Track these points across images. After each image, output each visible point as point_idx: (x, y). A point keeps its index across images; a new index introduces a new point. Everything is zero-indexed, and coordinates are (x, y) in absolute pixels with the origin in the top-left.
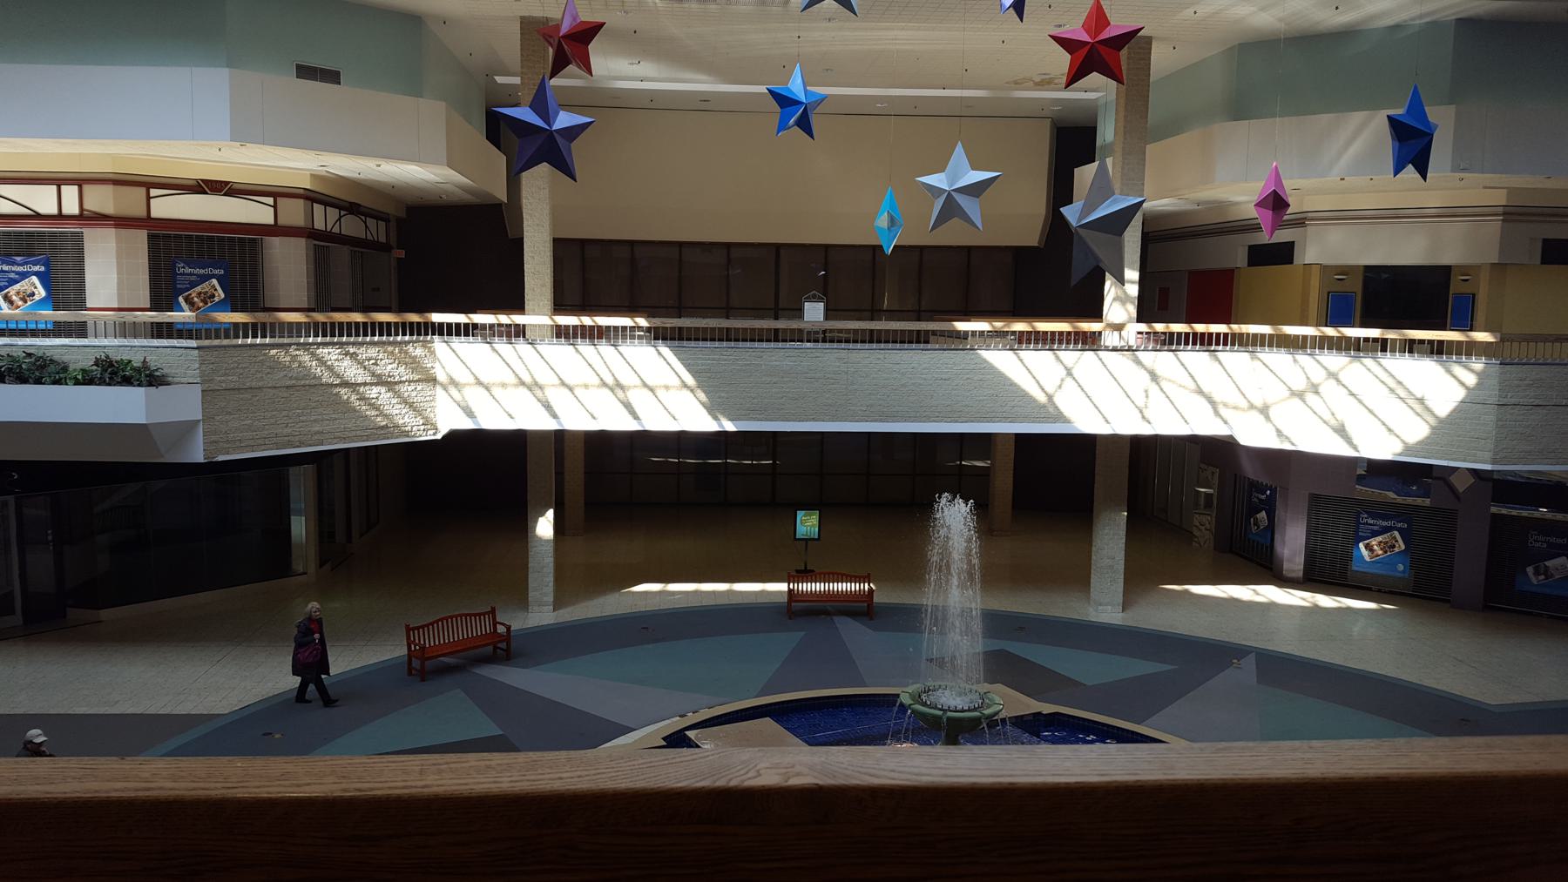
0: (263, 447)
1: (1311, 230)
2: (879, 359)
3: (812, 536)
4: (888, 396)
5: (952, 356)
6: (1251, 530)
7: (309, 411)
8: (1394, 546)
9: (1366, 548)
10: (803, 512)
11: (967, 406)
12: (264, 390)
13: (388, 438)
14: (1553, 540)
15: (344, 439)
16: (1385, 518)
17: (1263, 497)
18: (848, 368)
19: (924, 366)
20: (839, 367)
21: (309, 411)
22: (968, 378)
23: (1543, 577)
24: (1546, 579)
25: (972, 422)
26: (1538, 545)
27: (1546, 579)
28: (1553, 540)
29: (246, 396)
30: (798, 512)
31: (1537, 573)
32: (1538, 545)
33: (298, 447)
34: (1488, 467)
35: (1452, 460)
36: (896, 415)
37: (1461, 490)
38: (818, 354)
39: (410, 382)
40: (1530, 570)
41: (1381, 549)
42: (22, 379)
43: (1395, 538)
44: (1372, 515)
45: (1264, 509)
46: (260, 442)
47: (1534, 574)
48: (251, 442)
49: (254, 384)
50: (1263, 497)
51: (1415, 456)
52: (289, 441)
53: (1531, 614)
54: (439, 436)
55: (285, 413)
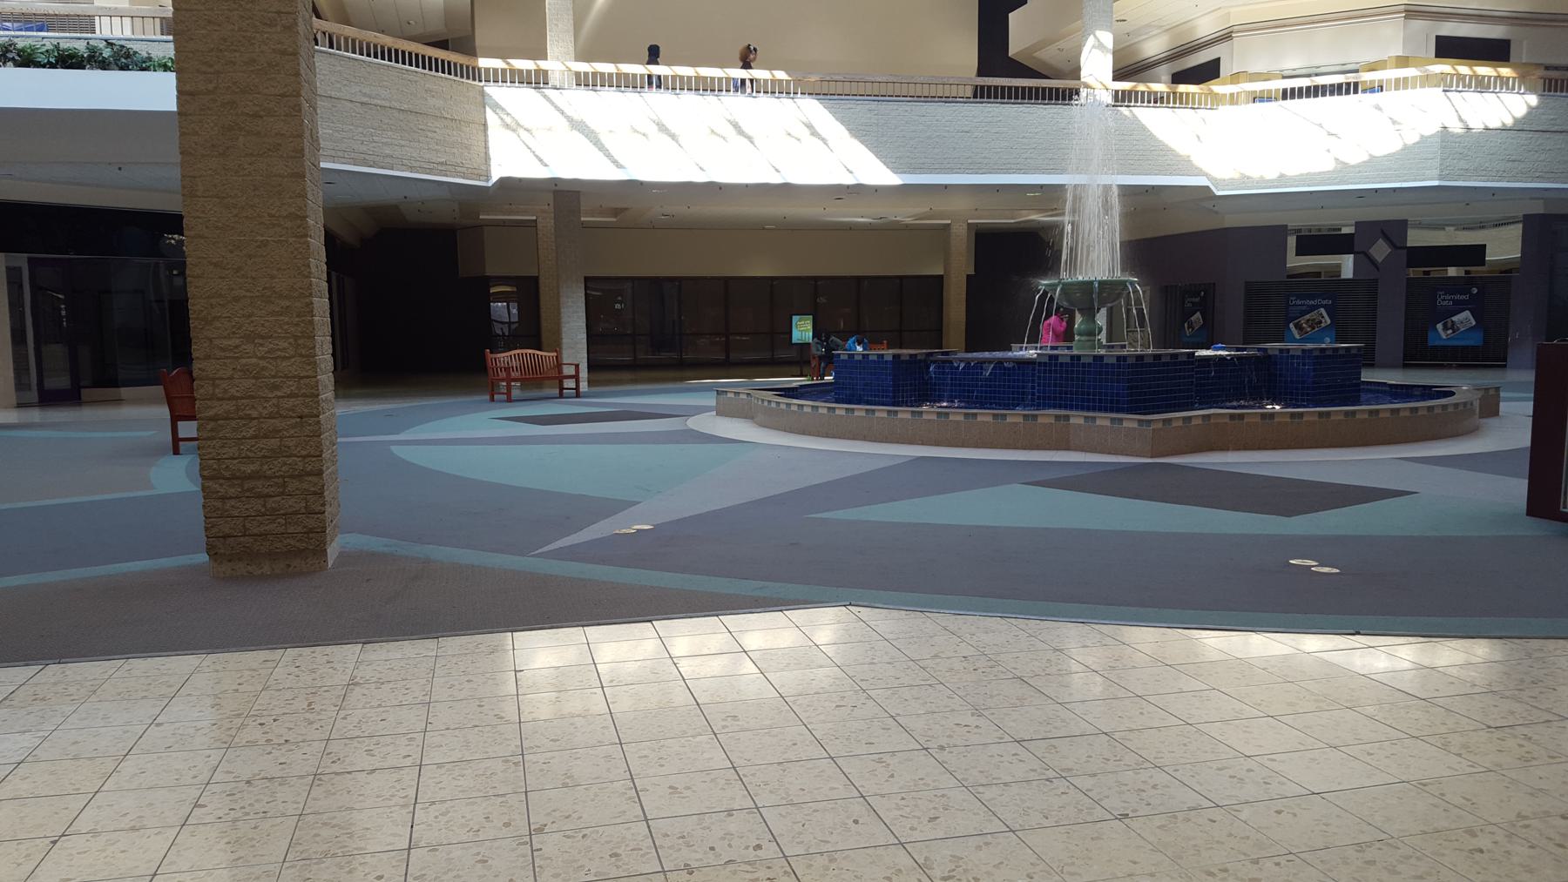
0: (343, 160)
1: (1237, 41)
2: (907, 111)
3: (807, 341)
4: (915, 148)
5: (973, 109)
6: (1185, 333)
7: (380, 132)
8: (1321, 322)
9: (1296, 328)
10: (798, 317)
11: (985, 158)
12: (343, 102)
13: (447, 176)
14: (1458, 297)
15: (412, 169)
16: (1312, 297)
17: (1197, 300)
18: (878, 120)
19: (947, 118)
20: (870, 118)
21: (380, 132)
22: (986, 131)
23: (1450, 332)
24: (1454, 332)
25: (990, 173)
26: (1445, 303)
27: (1454, 332)
28: (1458, 297)
29: (326, 104)
30: (794, 317)
31: (1445, 328)
32: (1445, 303)
33: (371, 166)
34: (1436, 183)
35: (1405, 181)
36: (922, 166)
37: (1380, 260)
38: (851, 106)
39: (222, 379)
40: (1440, 326)
41: (1310, 326)
42: (104, 65)
43: (1321, 314)
44: (1299, 297)
45: (1198, 310)
46: (340, 154)
47: (1443, 329)
48: (333, 153)
49: (333, 94)
50: (1197, 300)
51: (1373, 183)
52: (365, 159)
53: (1501, 273)
54: (490, 184)
55: (360, 130)
